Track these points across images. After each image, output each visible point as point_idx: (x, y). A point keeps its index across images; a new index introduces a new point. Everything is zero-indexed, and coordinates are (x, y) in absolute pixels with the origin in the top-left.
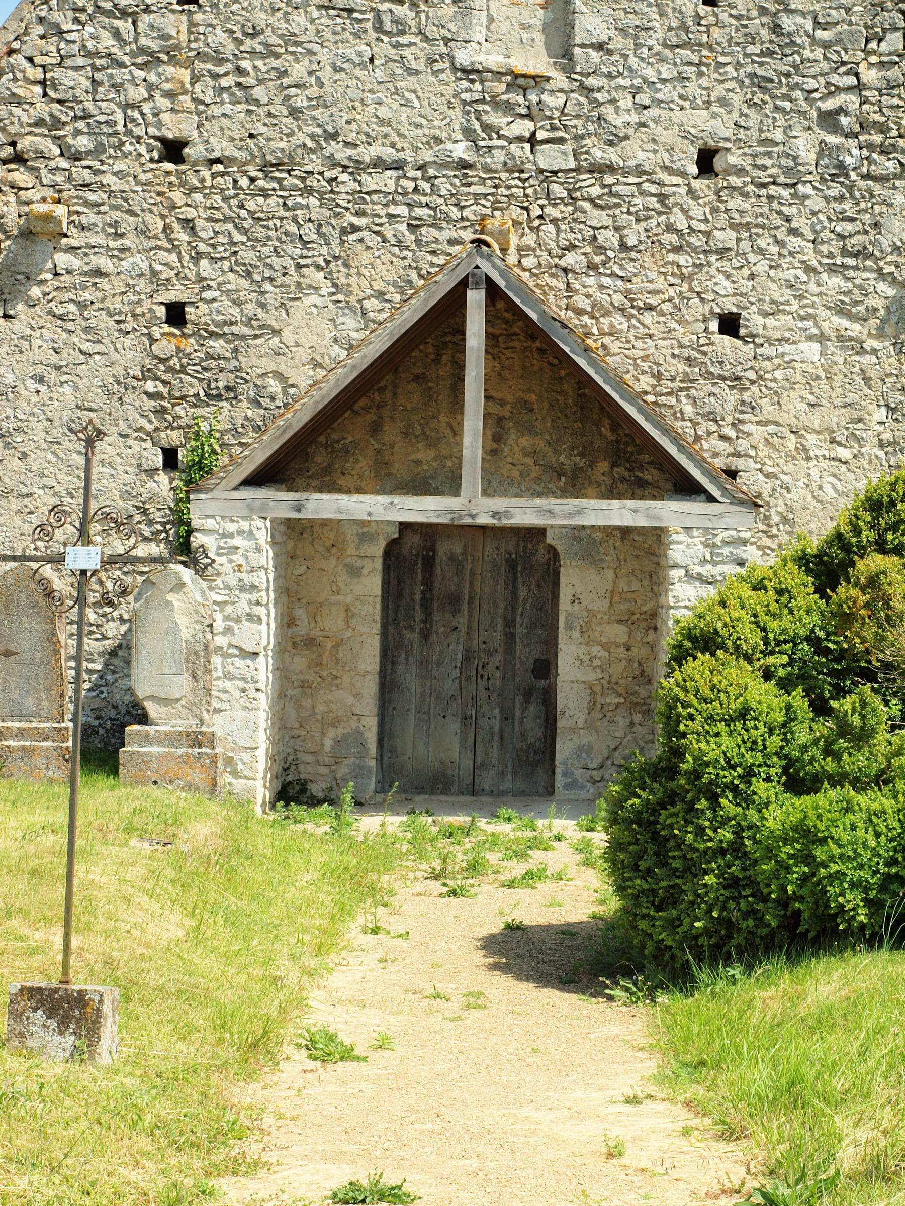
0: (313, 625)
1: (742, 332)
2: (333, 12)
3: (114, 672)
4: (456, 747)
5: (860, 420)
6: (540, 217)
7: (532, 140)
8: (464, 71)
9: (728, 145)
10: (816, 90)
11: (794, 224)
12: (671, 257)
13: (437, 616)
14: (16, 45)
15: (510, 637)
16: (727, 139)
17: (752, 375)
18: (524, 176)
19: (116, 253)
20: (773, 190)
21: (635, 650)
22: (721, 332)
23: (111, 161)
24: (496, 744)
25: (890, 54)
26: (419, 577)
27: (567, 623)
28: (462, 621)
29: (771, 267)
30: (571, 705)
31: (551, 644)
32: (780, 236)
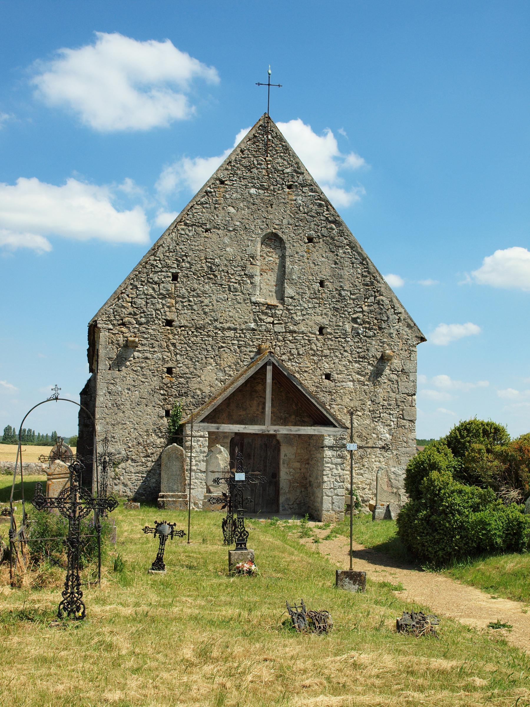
3: (150, 477)
5: (364, 404)
6: (275, 345)
7: (273, 323)
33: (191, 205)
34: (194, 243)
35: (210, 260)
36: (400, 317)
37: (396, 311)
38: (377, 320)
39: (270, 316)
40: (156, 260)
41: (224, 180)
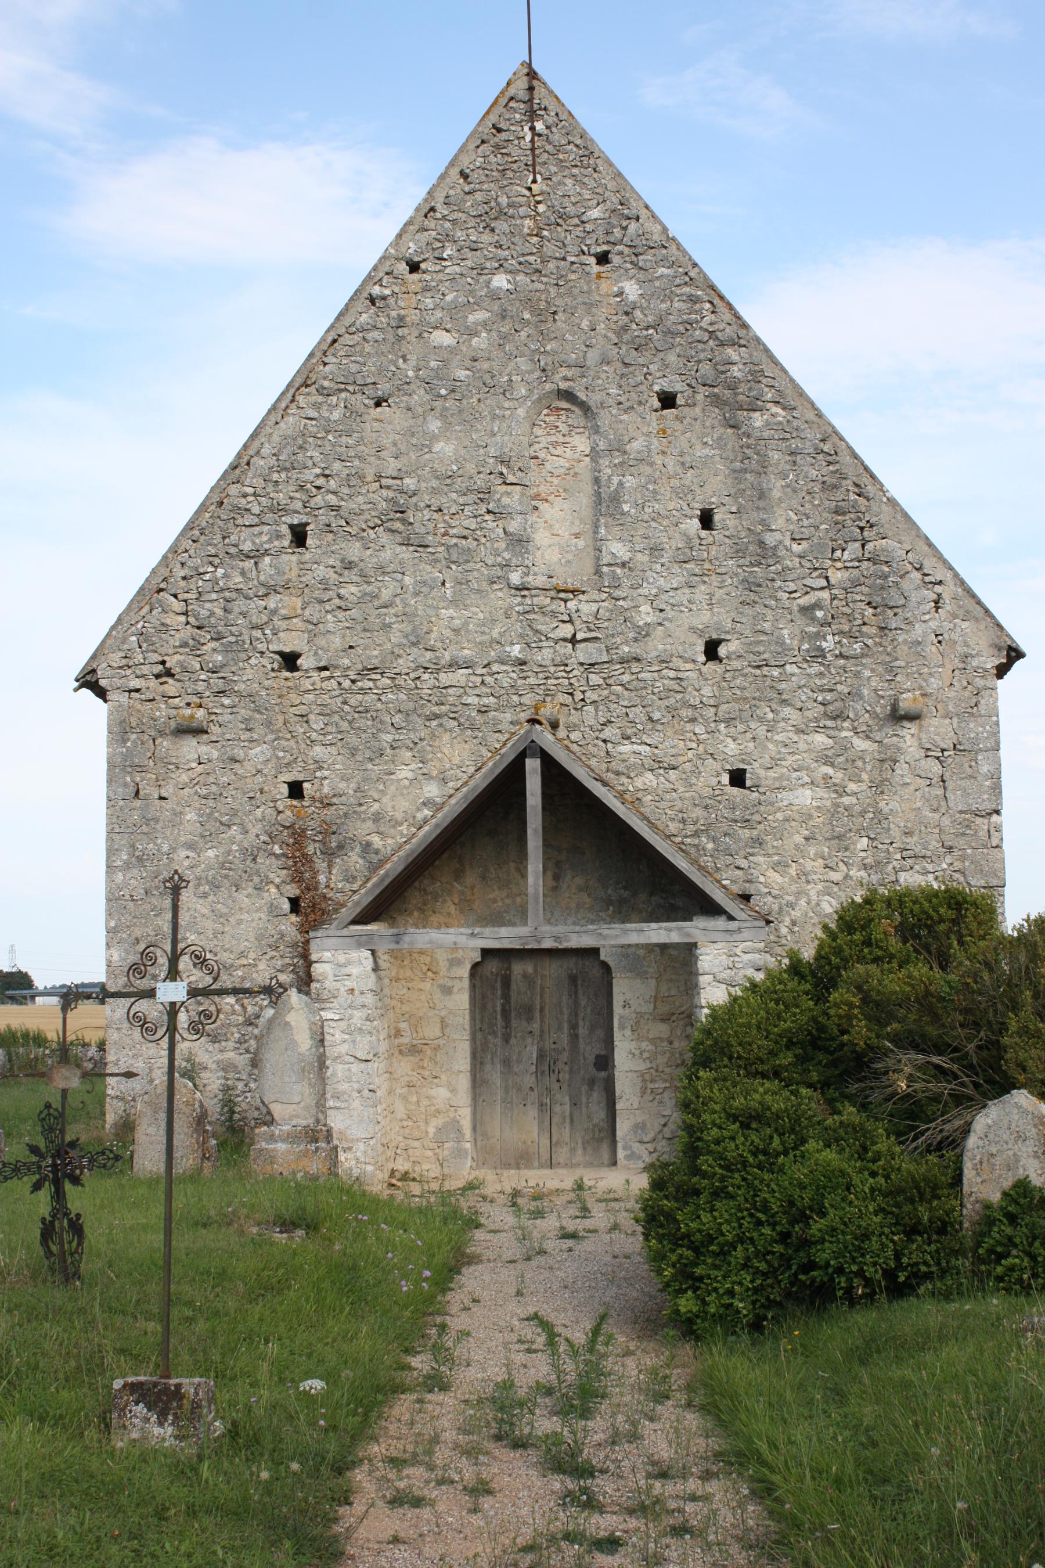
1: (748, 783)
2: (411, 548)
4: (536, 1128)
5: (847, 849)
6: (583, 700)
7: (573, 641)
9: (728, 637)
11: (784, 697)
12: (689, 727)
13: (514, 1023)
14: (163, 585)
15: (574, 1037)
17: (757, 817)
18: (568, 669)
21: (676, 1044)
24: (567, 1125)
28: (536, 1026)
30: (627, 1091)
32: (774, 706)
33: (330, 339)
35: (390, 482)
36: (939, 595)
39: (564, 622)
41: (416, 259)
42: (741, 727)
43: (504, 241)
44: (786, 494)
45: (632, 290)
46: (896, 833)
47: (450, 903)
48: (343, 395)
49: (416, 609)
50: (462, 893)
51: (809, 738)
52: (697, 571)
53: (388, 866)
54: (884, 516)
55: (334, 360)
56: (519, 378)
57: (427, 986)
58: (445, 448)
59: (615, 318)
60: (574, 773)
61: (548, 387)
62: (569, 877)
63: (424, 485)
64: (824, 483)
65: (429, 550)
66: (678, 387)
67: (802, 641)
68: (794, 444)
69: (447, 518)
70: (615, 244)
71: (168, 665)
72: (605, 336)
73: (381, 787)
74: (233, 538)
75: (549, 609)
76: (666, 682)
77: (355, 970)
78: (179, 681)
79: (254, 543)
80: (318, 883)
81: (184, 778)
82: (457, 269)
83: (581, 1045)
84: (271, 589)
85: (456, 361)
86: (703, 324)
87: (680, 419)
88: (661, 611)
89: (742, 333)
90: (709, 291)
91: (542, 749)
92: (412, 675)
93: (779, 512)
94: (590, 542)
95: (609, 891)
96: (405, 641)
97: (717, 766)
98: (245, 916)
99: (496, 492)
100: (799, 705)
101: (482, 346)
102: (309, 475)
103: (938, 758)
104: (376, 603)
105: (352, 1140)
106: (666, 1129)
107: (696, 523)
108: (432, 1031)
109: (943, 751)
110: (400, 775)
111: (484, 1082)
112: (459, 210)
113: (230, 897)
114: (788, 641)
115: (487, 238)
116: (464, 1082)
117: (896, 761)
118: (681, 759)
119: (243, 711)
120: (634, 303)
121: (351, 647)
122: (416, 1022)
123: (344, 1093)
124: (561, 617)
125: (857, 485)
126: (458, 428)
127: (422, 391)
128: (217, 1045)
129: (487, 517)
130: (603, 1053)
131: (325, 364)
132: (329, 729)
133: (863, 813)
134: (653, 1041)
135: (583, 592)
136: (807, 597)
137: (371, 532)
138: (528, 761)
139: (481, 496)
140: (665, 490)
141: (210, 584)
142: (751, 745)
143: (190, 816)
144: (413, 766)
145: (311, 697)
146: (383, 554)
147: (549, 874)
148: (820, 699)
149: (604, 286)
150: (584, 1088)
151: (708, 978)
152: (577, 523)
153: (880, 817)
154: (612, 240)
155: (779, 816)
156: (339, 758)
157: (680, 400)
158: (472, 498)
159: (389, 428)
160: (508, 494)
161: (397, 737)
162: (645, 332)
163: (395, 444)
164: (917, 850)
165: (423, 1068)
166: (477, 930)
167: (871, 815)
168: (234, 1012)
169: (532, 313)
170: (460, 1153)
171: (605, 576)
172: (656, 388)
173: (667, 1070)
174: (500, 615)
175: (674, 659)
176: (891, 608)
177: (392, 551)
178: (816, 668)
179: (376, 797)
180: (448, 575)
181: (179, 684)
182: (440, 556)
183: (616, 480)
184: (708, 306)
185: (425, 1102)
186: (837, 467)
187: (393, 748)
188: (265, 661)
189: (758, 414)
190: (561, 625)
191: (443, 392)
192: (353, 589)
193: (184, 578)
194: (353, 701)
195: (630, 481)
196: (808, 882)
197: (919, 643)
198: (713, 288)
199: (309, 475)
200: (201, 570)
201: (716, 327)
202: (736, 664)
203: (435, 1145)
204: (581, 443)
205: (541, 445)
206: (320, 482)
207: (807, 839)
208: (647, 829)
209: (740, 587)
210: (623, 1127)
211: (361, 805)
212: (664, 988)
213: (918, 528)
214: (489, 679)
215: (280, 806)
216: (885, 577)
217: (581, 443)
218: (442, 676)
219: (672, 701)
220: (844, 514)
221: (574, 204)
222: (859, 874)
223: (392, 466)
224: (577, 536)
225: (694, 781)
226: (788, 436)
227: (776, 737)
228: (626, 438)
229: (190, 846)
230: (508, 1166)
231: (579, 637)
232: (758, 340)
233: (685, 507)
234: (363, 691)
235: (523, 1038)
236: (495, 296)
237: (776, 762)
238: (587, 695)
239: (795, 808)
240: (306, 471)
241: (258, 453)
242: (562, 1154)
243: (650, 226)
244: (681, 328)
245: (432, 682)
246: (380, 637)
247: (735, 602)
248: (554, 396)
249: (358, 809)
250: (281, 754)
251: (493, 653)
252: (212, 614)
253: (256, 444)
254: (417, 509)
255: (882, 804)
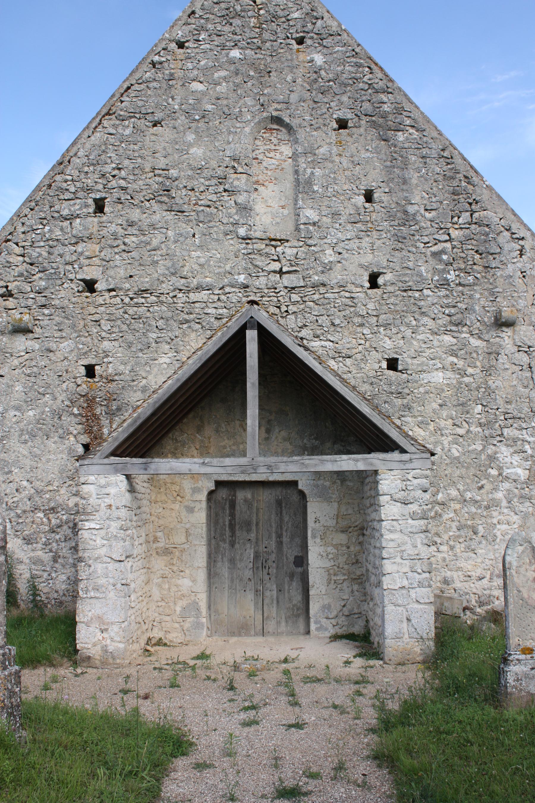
0: (167, 541)
1: (400, 368)
2: (173, 213)
3: (56, 572)
4: (252, 608)
5: (468, 413)
6: (287, 311)
7: (281, 272)
8: (243, 239)
9: (384, 271)
10: (428, 243)
11: (423, 310)
12: (359, 329)
13: (238, 533)
14: (9, 237)
15: (280, 543)
16: (384, 268)
17: (406, 391)
18: (277, 291)
19: (58, 340)
20: (410, 293)
21: (352, 549)
22: (389, 368)
23: (57, 293)
24: (275, 605)
25: (464, 224)
26: (228, 511)
27: (312, 534)
28: (253, 536)
29: (413, 333)
30: (317, 582)
31: (305, 547)
32: (417, 316)
33: (125, 87)
34: (132, 146)
35: (161, 172)
36: (523, 246)
37: (514, 236)
38: (481, 254)
39: (274, 260)
40: (66, 181)
41: (182, 40)
42: (394, 330)
43: (238, 31)
44: (421, 182)
45: (319, 59)
46: (500, 402)
47: (193, 448)
48: (133, 120)
49: (175, 251)
50: (202, 441)
51: (441, 338)
52: (363, 228)
53: (140, 410)
54: (485, 196)
55: (128, 99)
56: (246, 110)
57: (177, 506)
58: (197, 152)
59: (308, 75)
60: (283, 341)
61: (265, 114)
62: (277, 431)
63: (182, 173)
64: (445, 175)
65: (185, 214)
66: (349, 116)
67: (434, 274)
68: (424, 152)
69: (197, 194)
70: (308, 33)
71: (9, 288)
72: (302, 86)
73: (148, 369)
74: (57, 207)
75: (264, 251)
76: (343, 300)
77: (112, 491)
78: (17, 298)
79: (70, 210)
80: (102, 434)
81: (16, 362)
82: (208, 46)
83: (285, 549)
84: (80, 239)
85: (205, 100)
86: (365, 79)
87: (350, 135)
88: (340, 253)
89: (390, 84)
90: (368, 60)
91: (258, 323)
92: (171, 294)
93: (416, 192)
94: (292, 211)
95: (305, 441)
96: (167, 272)
97: (379, 356)
98: (52, 457)
99: (229, 178)
100: (433, 316)
101: (223, 91)
102: (108, 168)
103: (526, 352)
104: (148, 248)
105: (108, 624)
106: (345, 609)
107: (362, 199)
108: (179, 538)
109: (529, 347)
110: (161, 360)
111: (216, 574)
112: (210, 13)
113: (43, 443)
114: (425, 274)
115: (227, 28)
116: (202, 575)
117: (498, 354)
118: (354, 351)
119: (57, 318)
120: (321, 66)
121: (131, 276)
122: (168, 532)
123: (103, 586)
124: (272, 257)
125: (466, 177)
126: (206, 139)
127: (184, 117)
128: (30, 546)
129: (224, 194)
130: (300, 554)
131: (122, 102)
132: (114, 330)
133: (478, 389)
134: (336, 546)
135: (287, 241)
136: (436, 247)
137: (147, 203)
138: (248, 332)
139: (220, 180)
140: (341, 178)
141: (40, 236)
142: (402, 342)
143: (19, 388)
144: (170, 355)
145: (102, 309)
146: (154, 217)
147: (263, 429)
148: (447, 312)
149: (302, 56)
150: (287, 579)
151: (386, 498)
152: (283, 199)
153: (490, 391)
154: (306, 30)
155: (422, 390)
156: (120, 349)
157: (350, 124)
158: (214, 182)
159: (161, 139)
160: (238, 179)
161: (159, 335)
162: (327, 84)
163: (165, 149)
164: (515, 414)
165: (173, 564)
166: (207, 460)
167: (483, 390)
168: (42, 523)
169: (255, 71)
170: (198, 625)
171: (303, 232)
172: (335, 116)
173: (346, 567)
174: (231, 255)
175: (349, 285)
176: (492, 254)
177: (160, 215)
178: (443, 292)
179: (144, 375)
180: (197, 230)
181: (16, 301)
182: (192, 218)
183: (309, 171)
184: (367, 69)
185: (174, 589)
186: (453, 166)
187: (157, 343)
188: (73, 286)
189: (401, 133)
190: (272, 262)
191: (197, 117)
192: (134, 239)
193: (24, 233)
194: (131, 311)
195: (318, 172)
196: (442, 435)
197: (511, 277)
198: (370, 58)
199: (108, 168)
200: (35, 227)
201: (373, 81)
202: (390, 289)
203: (181, 620)
204: (286, 150)
205: (260, 151)
206: (116, 172)
207: (441, 406)
208: (339, 383)
209: (392, 239)
210: (314, 608)
211: (134, 381)
212: (343, 509)
213: (507, 204)
214: (223, 297)
215: (79, 381)
216: (487, 235)
217: (286, 150)
218: (191, 295)
219: (348, 312)
220: (458, 194)
221: (283, 10)
222: (476, 429)
223: (162, 163)
224: (283, 207)
225: (363, 365)
226: (421, 147)
227: (418, 337)
228: (316, 146)
229: (18, 408)
230: (233, 634)
231: (284, 269)
232: (400, 89)
233: (355, 188)
234: (137, 305)
235: (244, 544)
236: (232, 62)
237: (419, 353)
238: (290, 308)
239: (432, 385)
240: (106, 166)
241: (76, 154)
242: (271, 626)
243: (330, 22)
244: (351, 82)
245: (185, 299)
246: (150, 270)
247: (389, 249)
248: (268, 121)
249: (132, 384)
250: (81, 346)
251: (226, 280)
252: (40, 255)
253: (75, 149)
254: (178, 189)
255: (490, 383)
